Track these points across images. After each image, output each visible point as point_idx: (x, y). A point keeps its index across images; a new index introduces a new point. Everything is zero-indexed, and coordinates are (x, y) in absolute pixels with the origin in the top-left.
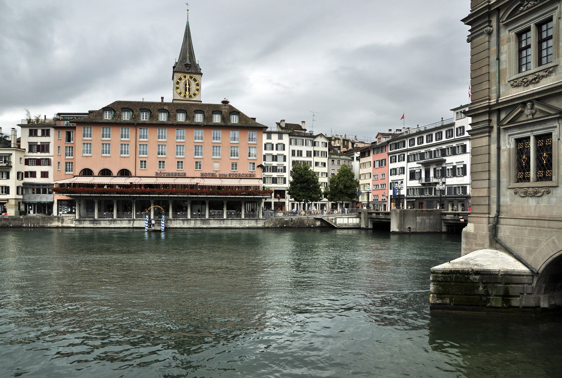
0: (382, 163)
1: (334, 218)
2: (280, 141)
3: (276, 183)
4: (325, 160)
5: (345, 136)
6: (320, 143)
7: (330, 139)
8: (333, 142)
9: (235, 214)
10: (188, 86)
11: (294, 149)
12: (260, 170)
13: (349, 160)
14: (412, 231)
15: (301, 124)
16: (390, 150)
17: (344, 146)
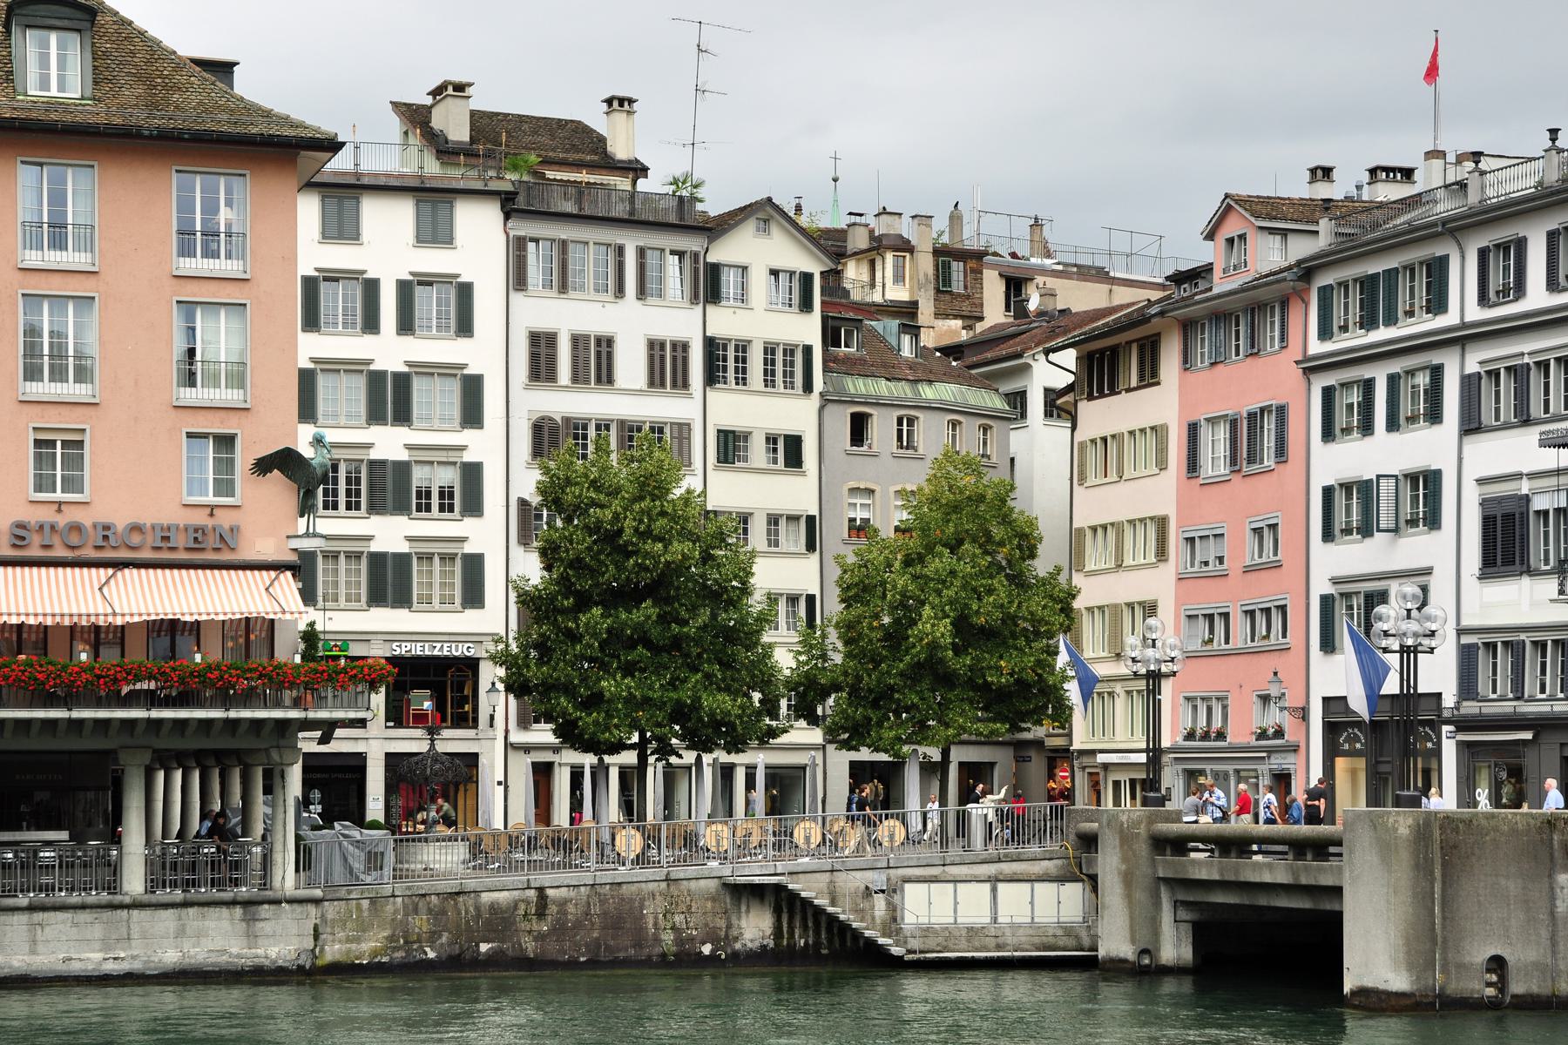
0: (1255, 437)
1: (878, 879)
2: (434, 261)
3: (402, 599)
4: (795, 413)
5: (955, 218)
6: (759, 282)
7: (832, 245)
8: (854, 273)
9: (66, 866)
11: (543, 324)
12: (278, 490)
13: (987, 419)
14: (1517, 987)
15: (596, 119)
16: (1325, 333)
17: (950, 302)
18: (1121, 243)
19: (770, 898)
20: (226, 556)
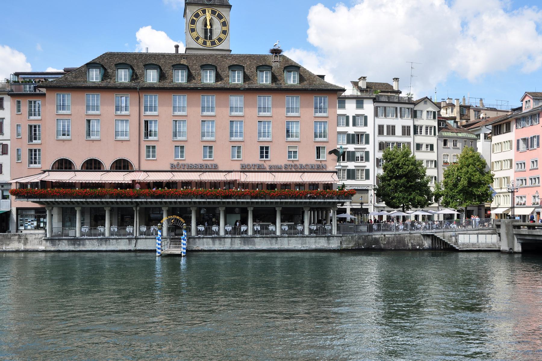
2: (360, 112)
5: (464, 99)
6: (425, 113)
10: (209, 27)
11: (381, 124)
18: (499, 103)
19: (431, 237)
20: (324, 170)
